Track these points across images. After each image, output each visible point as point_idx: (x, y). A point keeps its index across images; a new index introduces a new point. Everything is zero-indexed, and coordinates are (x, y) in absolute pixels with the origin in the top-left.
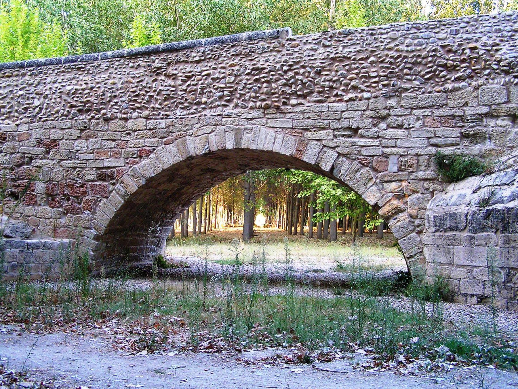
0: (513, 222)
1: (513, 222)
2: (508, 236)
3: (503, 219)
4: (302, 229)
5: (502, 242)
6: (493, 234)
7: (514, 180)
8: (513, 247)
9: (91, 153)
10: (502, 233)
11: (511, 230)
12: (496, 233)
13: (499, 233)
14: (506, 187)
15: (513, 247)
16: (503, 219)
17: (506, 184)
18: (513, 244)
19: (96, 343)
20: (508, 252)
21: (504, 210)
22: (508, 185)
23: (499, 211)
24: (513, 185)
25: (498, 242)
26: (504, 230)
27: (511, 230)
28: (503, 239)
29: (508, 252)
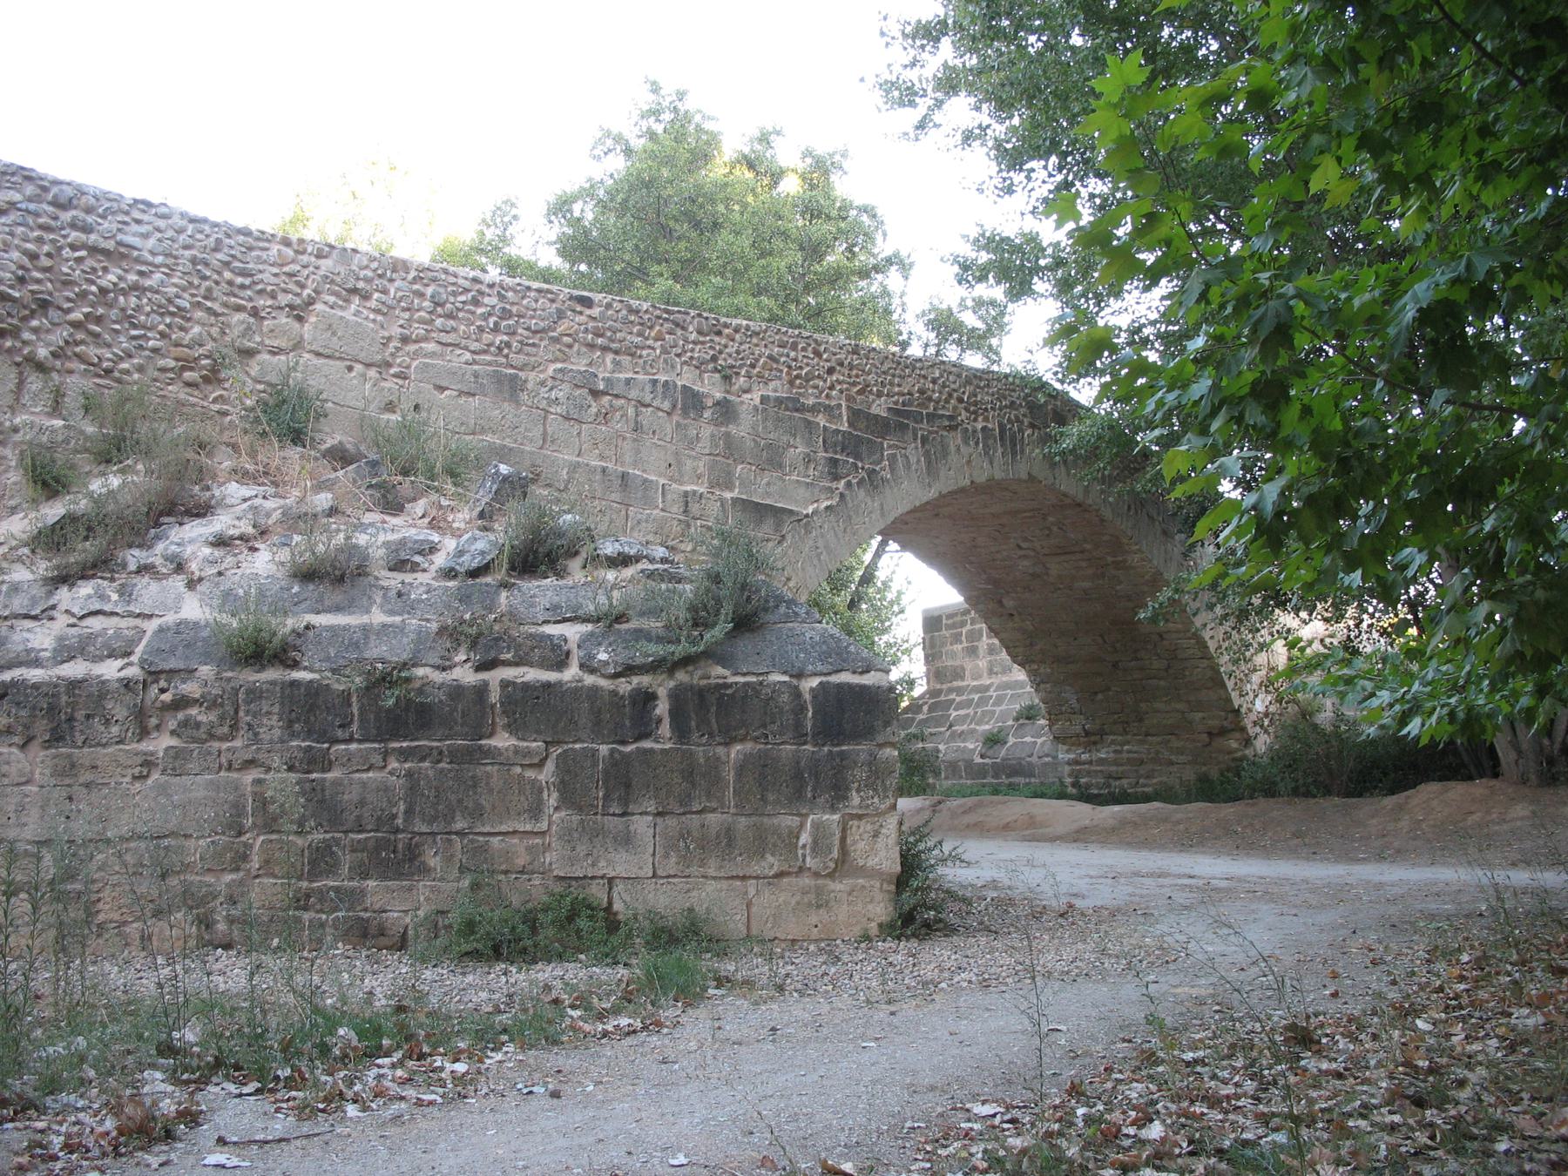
0: (88, 717)
1: (88, 717)
2: (69, 756)
3: (52, 710)
4: (1517, 78)
5: (47, 772)
6: (14, 750)
7: (53, 607)
8: (87, 785)
9: (619, 815)
10: (47, 748)
11: (80, 739)
12: (23, 747)
13: (34, 747)
14: (28, 624)
15: (87, 785)
16: (52, 710)
17: (27, 617)
18: (87, 777)
19: (31, 492)
20: (70, 798)
21: (56, 686)
22: (35, 618)
23: (36, 686)
24: (52, 619)
25: (32, 773)
26: (56, 738)
27: (80, 739)
28: (48, 762)
29: (70, 798)
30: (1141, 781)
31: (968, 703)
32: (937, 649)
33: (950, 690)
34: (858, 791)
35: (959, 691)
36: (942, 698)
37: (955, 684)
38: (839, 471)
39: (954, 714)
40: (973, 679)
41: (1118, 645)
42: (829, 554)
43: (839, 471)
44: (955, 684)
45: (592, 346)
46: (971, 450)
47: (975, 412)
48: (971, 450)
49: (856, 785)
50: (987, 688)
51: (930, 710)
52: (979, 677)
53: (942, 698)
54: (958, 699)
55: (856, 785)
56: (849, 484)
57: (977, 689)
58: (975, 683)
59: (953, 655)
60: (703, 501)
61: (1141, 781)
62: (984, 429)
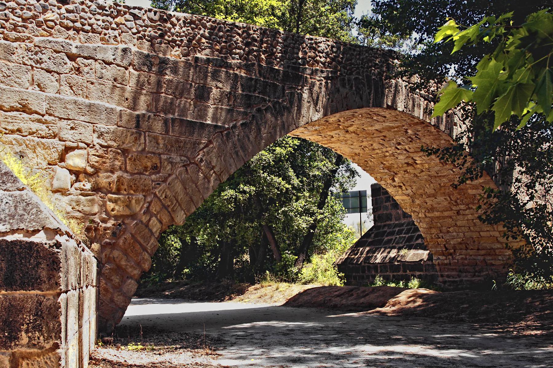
30: (476, 274)
31: (392, 233)
32: (379, 205)
33: (385, 226)
34: (27, 331)
35: (389, 226)
36: (381, 230)
37: (388, 223)
38: (252, 102)
39: (386, 239)
40: (396, 220)
41: (458, 201)
42: (244, 151)
43: (252, 102)
44: (388, 223)
45: (68, 28)
46: (347, 91)
47: (350, 69)
48: (347, 91)
49: (25, 326)
50: (402, 225)
51: (375, 237)
52: (400, 219)
53: (381, 230)
54: (388, 231)
55: (25, 326)
56: (259, 110)
57: (396, 226)
58: (397, 222)
59: (386, 208)
60: (151, 121)
61: (476, 274)
62: (356, 79)
